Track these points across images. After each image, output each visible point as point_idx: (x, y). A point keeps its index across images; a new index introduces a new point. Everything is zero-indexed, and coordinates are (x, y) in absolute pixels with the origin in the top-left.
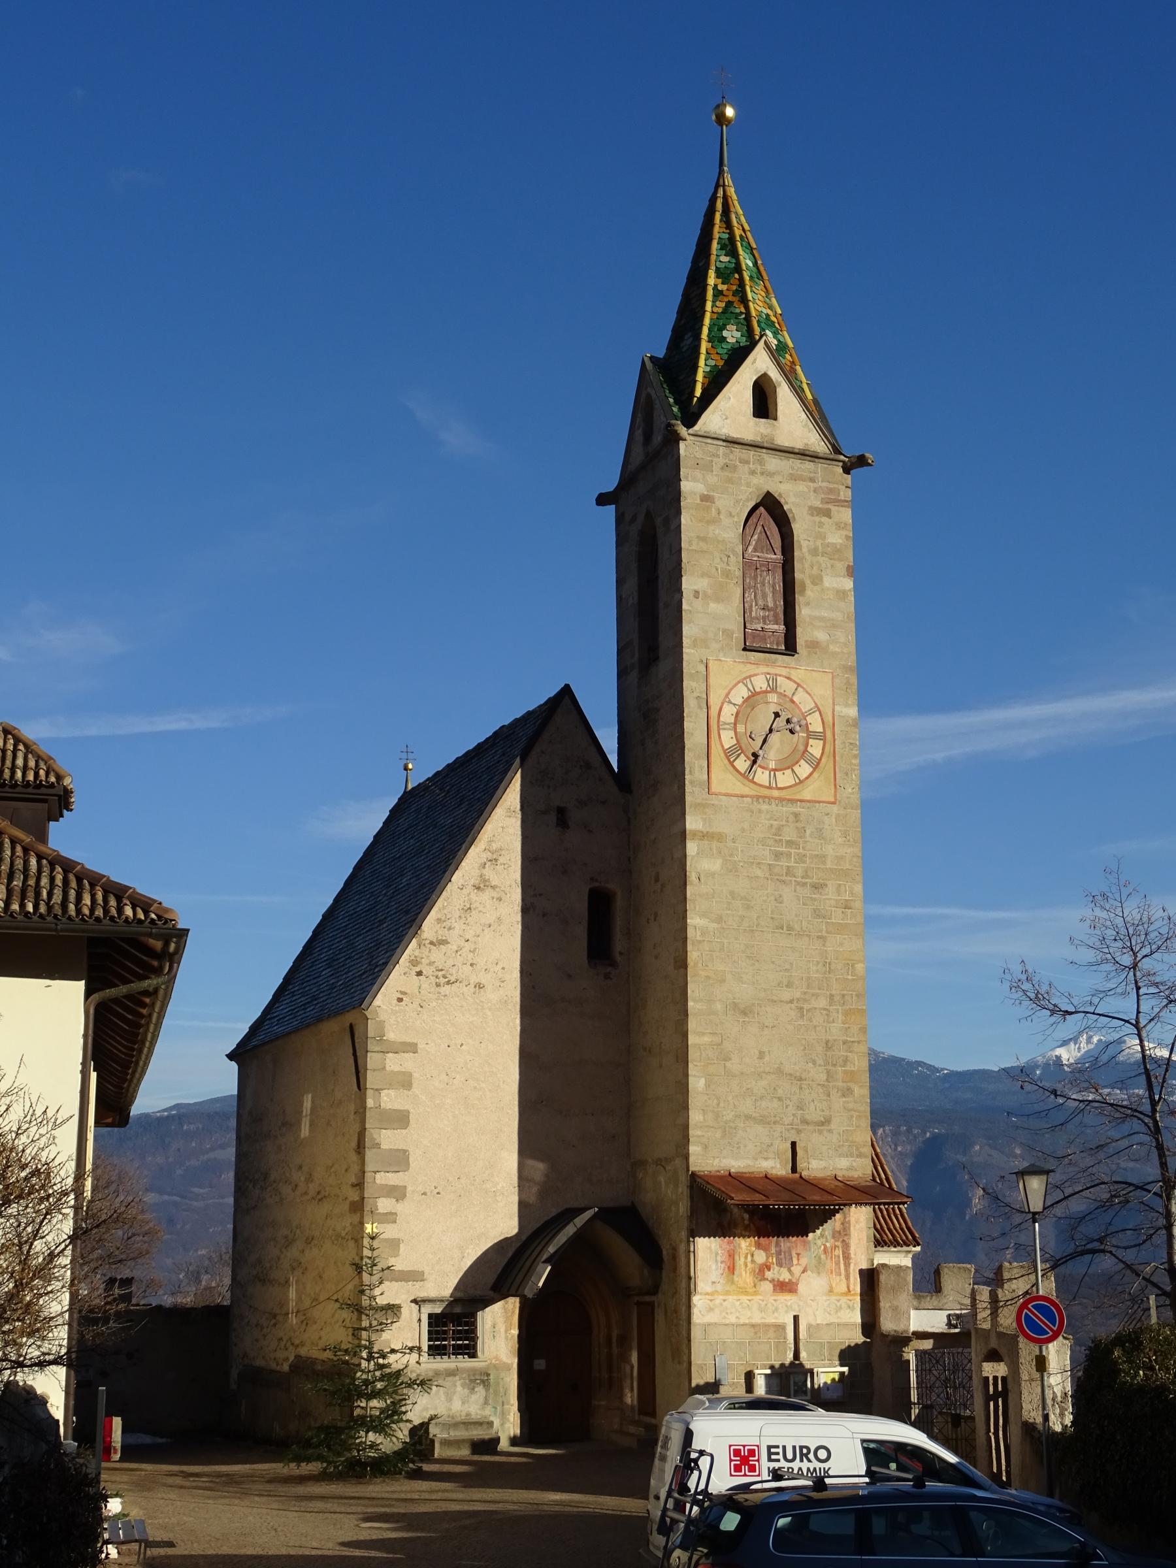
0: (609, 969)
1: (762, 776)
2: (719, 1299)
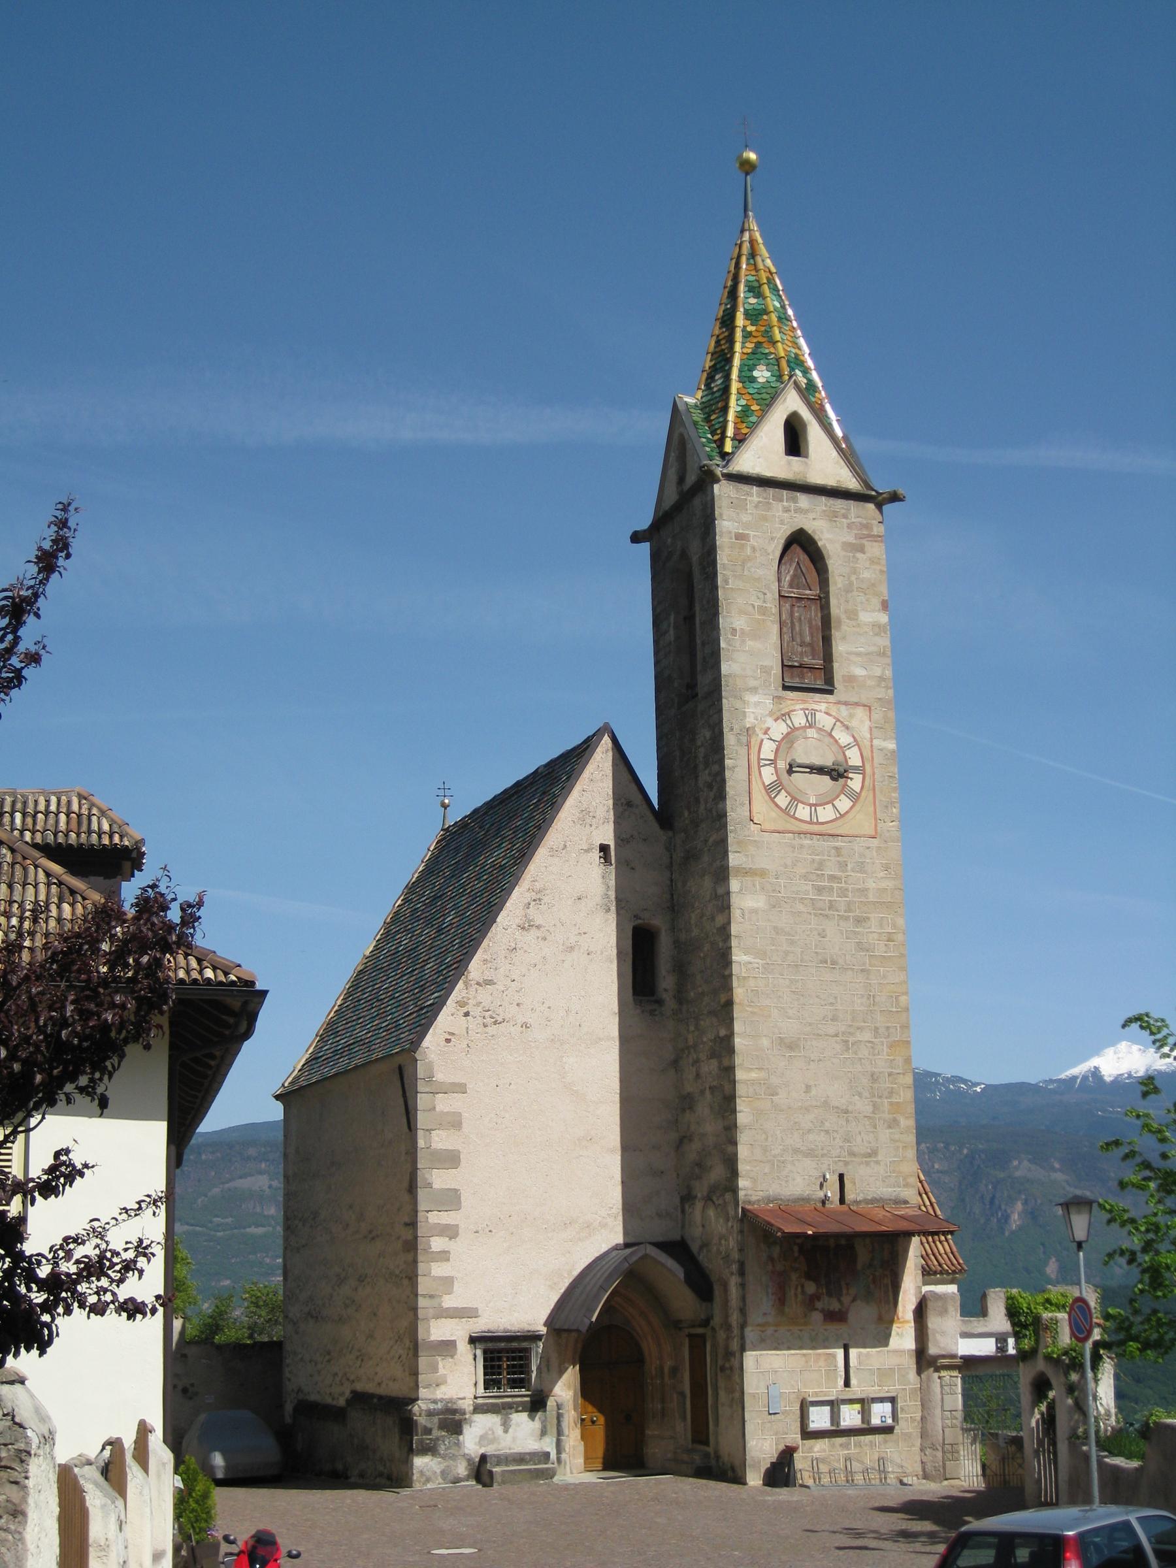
1: (803, 812)
2: (770, 1330)
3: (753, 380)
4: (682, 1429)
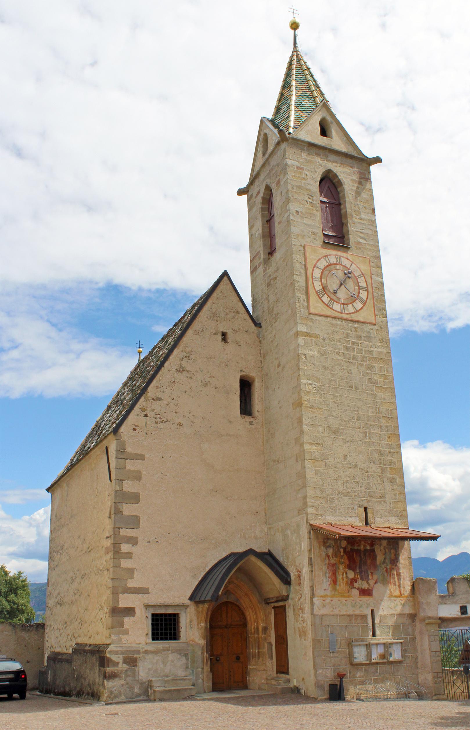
0: (252, 420)
2: (328, 600)
4: (271, 664)
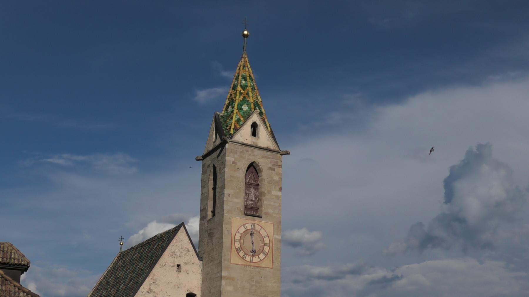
3: (242, 109)
